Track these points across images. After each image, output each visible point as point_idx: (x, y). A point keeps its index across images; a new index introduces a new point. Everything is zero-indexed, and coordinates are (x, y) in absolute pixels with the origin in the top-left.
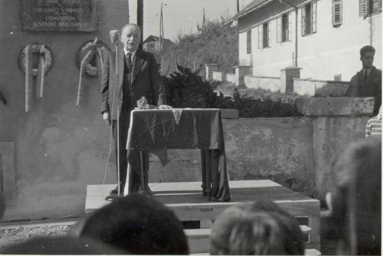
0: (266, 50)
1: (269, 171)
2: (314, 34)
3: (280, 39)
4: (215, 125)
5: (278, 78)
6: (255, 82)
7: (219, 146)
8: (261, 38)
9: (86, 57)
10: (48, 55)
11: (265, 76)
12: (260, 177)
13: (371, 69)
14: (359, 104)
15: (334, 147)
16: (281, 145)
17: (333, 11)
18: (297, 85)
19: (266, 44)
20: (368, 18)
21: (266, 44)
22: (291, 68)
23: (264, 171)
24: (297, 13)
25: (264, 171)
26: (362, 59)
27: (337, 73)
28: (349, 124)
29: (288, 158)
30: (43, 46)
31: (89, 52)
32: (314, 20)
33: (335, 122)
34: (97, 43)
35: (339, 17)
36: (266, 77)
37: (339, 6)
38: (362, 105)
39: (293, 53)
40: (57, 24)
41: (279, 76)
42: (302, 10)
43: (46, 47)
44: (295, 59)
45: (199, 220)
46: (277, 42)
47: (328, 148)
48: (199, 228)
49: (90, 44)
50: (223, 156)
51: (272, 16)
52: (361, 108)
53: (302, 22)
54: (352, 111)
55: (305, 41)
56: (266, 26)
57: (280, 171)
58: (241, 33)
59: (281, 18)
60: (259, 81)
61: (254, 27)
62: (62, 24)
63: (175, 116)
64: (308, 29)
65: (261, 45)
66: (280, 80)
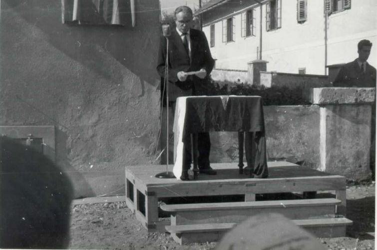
0: (230, 44)
1: (281, 154)
2: (279, 29)
3: (244, 33)
4: (257, 110)
5: (245, 71)
6: (221, 74)
7: (261, 129)
8: (225, 31)
11: (231, 69)
12: (282, 159)
14: (362, 94)
15: (340, 132)
16: (292, 131)
17: (297, 8)
18: (264, 78)
19: (230, 38)
21: (230, 38)
22: (256, 61)
23: (277, 153)
24: (261, 9)
25: (277, 153)
26: (359, 52)
27: (302, 67)
28: (353, 111)
29: (299, 142)
32: (279, 16)
33: (340, 110)
35: (304, 14)
36: (232, 70)
37: (304, 3)
38: (364, 94)
39: (258, 47)
41: (246, 70)
42: (267, 6)
44: (259, 53)
45: (243, 193)
46: (223, 42)
47: (335, 133)
48: (244, 201)
50: (264, 138)
51: (236, 11)
52: (364, 97)
53: (266, 18)
54: (356, 100)
55: (269, 36)
56: (230, 21)
57: (291, 154)
58: (205, 26)
59: (245, 13)
60: (225, 74)
61: (217, 22)
63: (223, 102)
64: (273, 25)
65: (225, 39)
66: (247, 73)
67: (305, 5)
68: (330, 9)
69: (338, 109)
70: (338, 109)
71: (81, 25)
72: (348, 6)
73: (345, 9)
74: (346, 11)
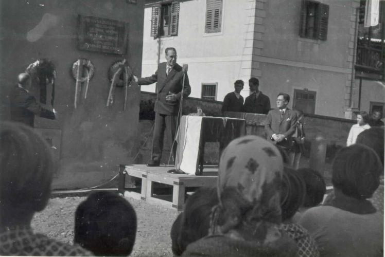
9: (117, 73)
10: (92, 69)
13: (259, 93)
20: (158, 39)
26: (235, 87)
30: (89, 62)
31: (120, 69)
33: (256, 130)
34: (125, 63)
40: (102, 46)
43: (91, 63)
49: (120, 63)
62: (104, 47)
67: (219, 14)
68: (158, 24)
69: (255, 129)
70: (255, 129)
71: (358, 39)
72: (175, 33)
73: (172, 35)
74: (173, 37)
